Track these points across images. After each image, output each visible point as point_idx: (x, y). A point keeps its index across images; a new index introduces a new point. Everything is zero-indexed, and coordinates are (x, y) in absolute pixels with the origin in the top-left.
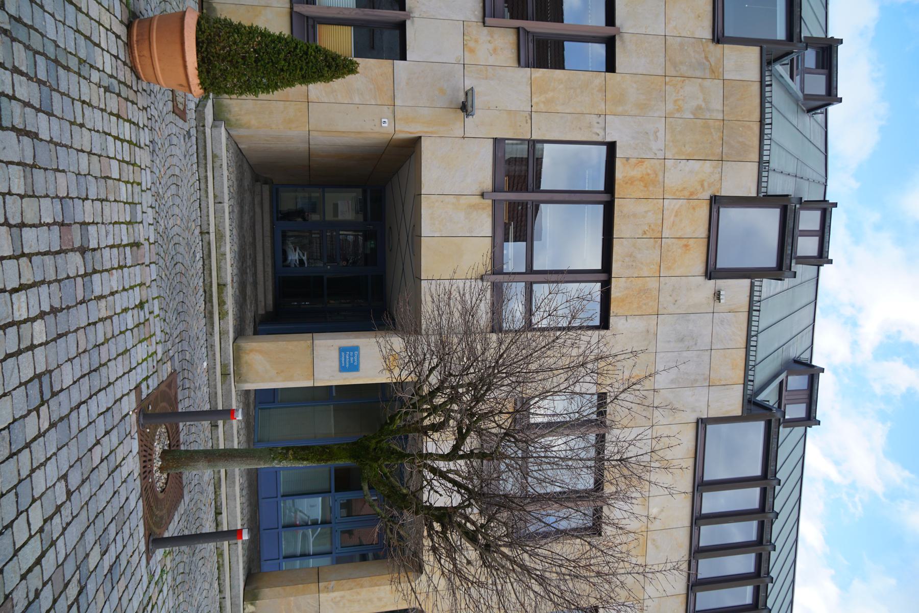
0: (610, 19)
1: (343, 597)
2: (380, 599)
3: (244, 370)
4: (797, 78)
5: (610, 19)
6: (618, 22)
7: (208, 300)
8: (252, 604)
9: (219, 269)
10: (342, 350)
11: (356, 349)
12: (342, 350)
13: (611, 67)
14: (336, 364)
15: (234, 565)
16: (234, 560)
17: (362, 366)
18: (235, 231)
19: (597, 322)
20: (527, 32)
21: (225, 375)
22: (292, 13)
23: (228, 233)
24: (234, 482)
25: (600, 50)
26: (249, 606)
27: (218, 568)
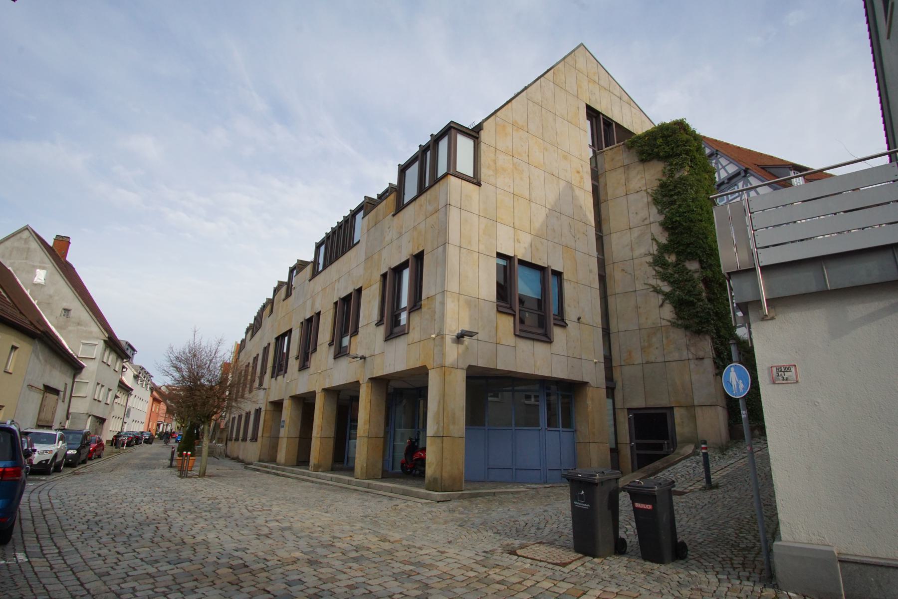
24: (412, 491)
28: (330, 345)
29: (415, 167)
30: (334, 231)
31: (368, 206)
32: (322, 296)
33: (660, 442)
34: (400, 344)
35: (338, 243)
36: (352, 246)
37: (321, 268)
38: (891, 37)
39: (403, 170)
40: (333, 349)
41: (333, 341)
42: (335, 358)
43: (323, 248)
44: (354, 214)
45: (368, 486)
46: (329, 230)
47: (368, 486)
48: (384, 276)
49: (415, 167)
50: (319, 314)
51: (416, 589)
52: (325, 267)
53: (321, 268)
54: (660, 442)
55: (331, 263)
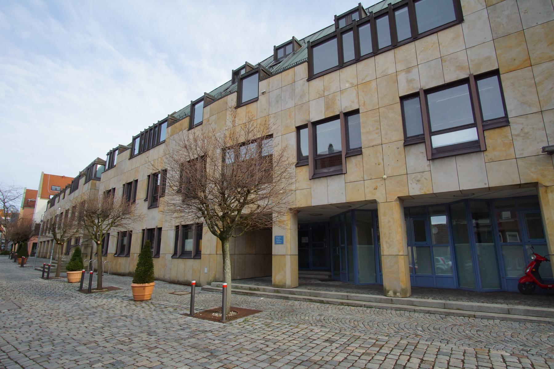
0: (336, 117)
1: (387, 242)
2: (389, 222)
3: (281, 284)
4: (281, 60)
5: (336, 117)
6: (337, 113)
7: (252, 294)
8: (388, 292)
9: (245, 289)
10: (276, 244)
11: (275, 237)
12: (276, 244)
13: (356, 112)
14: (280, 245)
15: (359, 299)
16: (355, 298)
17: (282, 235)
18: (308, 287)
19: (496, 78)
20: (347, 153)
21: (278, 292)
22: (194, 258)
23: (480, 304)
24: (319, 293)
25: (351, 118)
26: (389, 294)
27: (348, 306)
28: (145, 200)
29: (139, 139)
30: (146, 131)
31: (171, 120)
32: (140, 169)
33: (346, 242)
34: (155, 212)
35: (149, 138)
36: (159, 143)
37: (136, 152)
38: (355, 107)
39: (134, 139)
40: (147, 203)
41: (147, 198)
42: (149, 208)
43: (138, 140)
44: (161, 123)
45: (412, 303)
46: (143, 130)
47: (412, 303)
48: (149, 176)
49: (139, 139)
50: (137, 181)
51: (203, 357)
52: (140, 153)
53: (136, 152)
54: (346, 242)
55: (144, 152)
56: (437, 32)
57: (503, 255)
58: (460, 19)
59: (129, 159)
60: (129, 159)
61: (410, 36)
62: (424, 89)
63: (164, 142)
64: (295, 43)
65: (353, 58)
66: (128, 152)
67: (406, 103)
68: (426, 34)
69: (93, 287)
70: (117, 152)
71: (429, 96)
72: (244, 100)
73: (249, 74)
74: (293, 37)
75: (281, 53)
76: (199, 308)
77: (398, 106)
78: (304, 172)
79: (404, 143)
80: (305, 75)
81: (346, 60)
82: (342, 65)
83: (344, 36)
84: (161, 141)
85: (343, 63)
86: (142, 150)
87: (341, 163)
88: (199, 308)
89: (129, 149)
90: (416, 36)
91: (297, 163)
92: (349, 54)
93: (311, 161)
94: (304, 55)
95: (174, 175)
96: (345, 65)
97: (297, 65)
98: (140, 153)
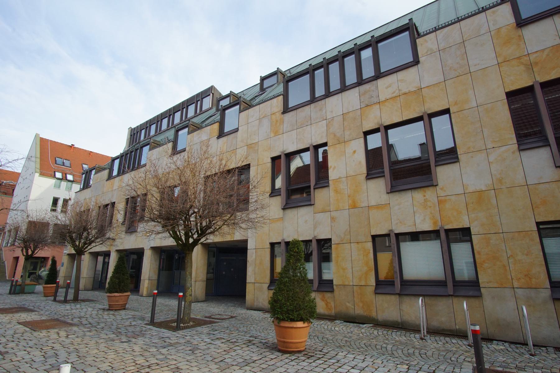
29: (118, 160)
36: (139, 166)
37: (115, 173)
41: (124, 221)
43: (117, 162)
49: (118, 160)
52: (119, 174)
53: (115, 173)
56: (296, 109)
57: (140, 139)
58: (416, 62)
59: (107, 181)
60: (107, 181)
61: (412, 60)
62: (385, 124)
63: (145, 165)
64: (280, 75)
65: (373, 74)
66: (106, 172)
67: (369, 137)
68: (304, 104)
69: (68, 298)
70: (93, 172)
71: (390, 131)
72: (226, 130)
73: (232, 104)
74: (278, 68)
75: (267, 83)
76: (159, 318)
77: (362, 140)
78: (277, 203)
79: (366, 177)
80: (170, 151)
81: (317, 96)
82: (313, 100)
83: (331, 66)
84: (178, 150)
85: (330, 92)
86: (121, 172)
87: (309, 193)
88: (159, 318)
89: (104, 169)
90: (379, 75)
91: (272, 193)
92: (320, 91)
93: (283, 192)
94: (280, 89)
95: (154, 200)
96: (363, 82)
97: (275, 97)
98: (119, 174)
